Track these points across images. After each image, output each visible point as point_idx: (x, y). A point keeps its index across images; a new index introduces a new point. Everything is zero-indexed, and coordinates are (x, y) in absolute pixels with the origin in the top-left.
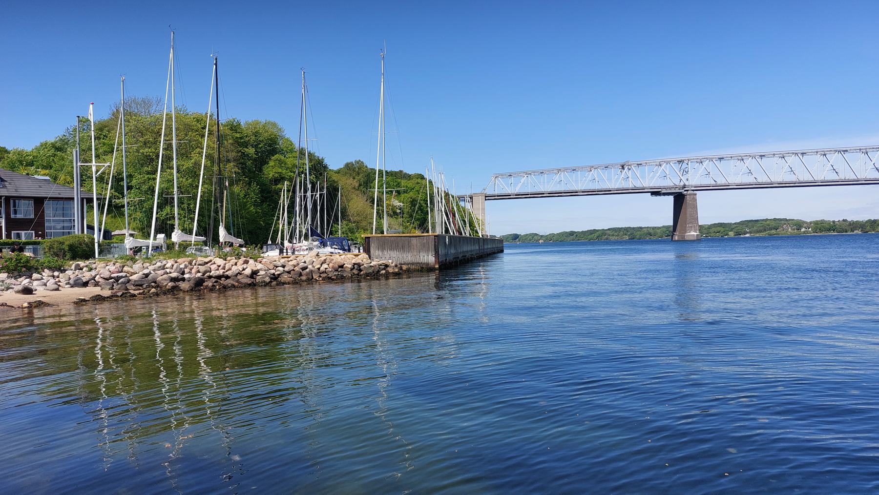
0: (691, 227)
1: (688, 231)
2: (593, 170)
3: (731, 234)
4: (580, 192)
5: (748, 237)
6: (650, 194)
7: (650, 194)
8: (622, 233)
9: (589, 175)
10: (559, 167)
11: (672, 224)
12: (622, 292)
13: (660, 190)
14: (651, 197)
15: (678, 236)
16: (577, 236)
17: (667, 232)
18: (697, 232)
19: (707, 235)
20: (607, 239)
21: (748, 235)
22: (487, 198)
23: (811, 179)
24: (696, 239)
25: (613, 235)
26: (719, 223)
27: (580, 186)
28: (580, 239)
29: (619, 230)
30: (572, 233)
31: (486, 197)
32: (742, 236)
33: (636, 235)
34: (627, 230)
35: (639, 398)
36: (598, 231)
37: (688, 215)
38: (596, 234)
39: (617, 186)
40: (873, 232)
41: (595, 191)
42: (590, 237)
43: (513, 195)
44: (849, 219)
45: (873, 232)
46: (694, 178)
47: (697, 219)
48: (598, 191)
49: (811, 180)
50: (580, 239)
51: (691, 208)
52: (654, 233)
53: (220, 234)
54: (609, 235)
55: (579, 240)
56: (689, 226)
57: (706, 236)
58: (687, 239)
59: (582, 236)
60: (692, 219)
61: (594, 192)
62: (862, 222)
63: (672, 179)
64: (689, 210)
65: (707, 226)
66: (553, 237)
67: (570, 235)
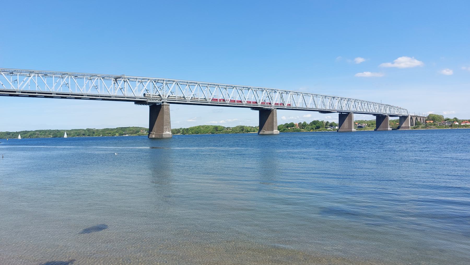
0: (167, 128)
1: (165, 131)
2: (32, 76)
3: (117, 134)
5: (127, 136)
6: (134, 103)
7: (134, 103)
8: (48, 133)
9: (27, 80)
10: (32, 69)
11: (148, 128)
12: (329, 174)
17: (78, 133)
19: (103, 135)
20: (37, 137)
24: (171, 137)
25: (41, 135)
26: (107, 129)
29: (45, 132)
32: (124, 136)
34: (50, 131)
36: (29, 132)
37: (164, 120)
38: (29, 134)
40: (187, 134)
45: (187, 134)
47: (170, 123)
54: (38, 135)
56: (165, 127)
57: (103, 136)
60: (167, 122)
62: (228, 128)
64: (165, 116)
67: (7, 134)
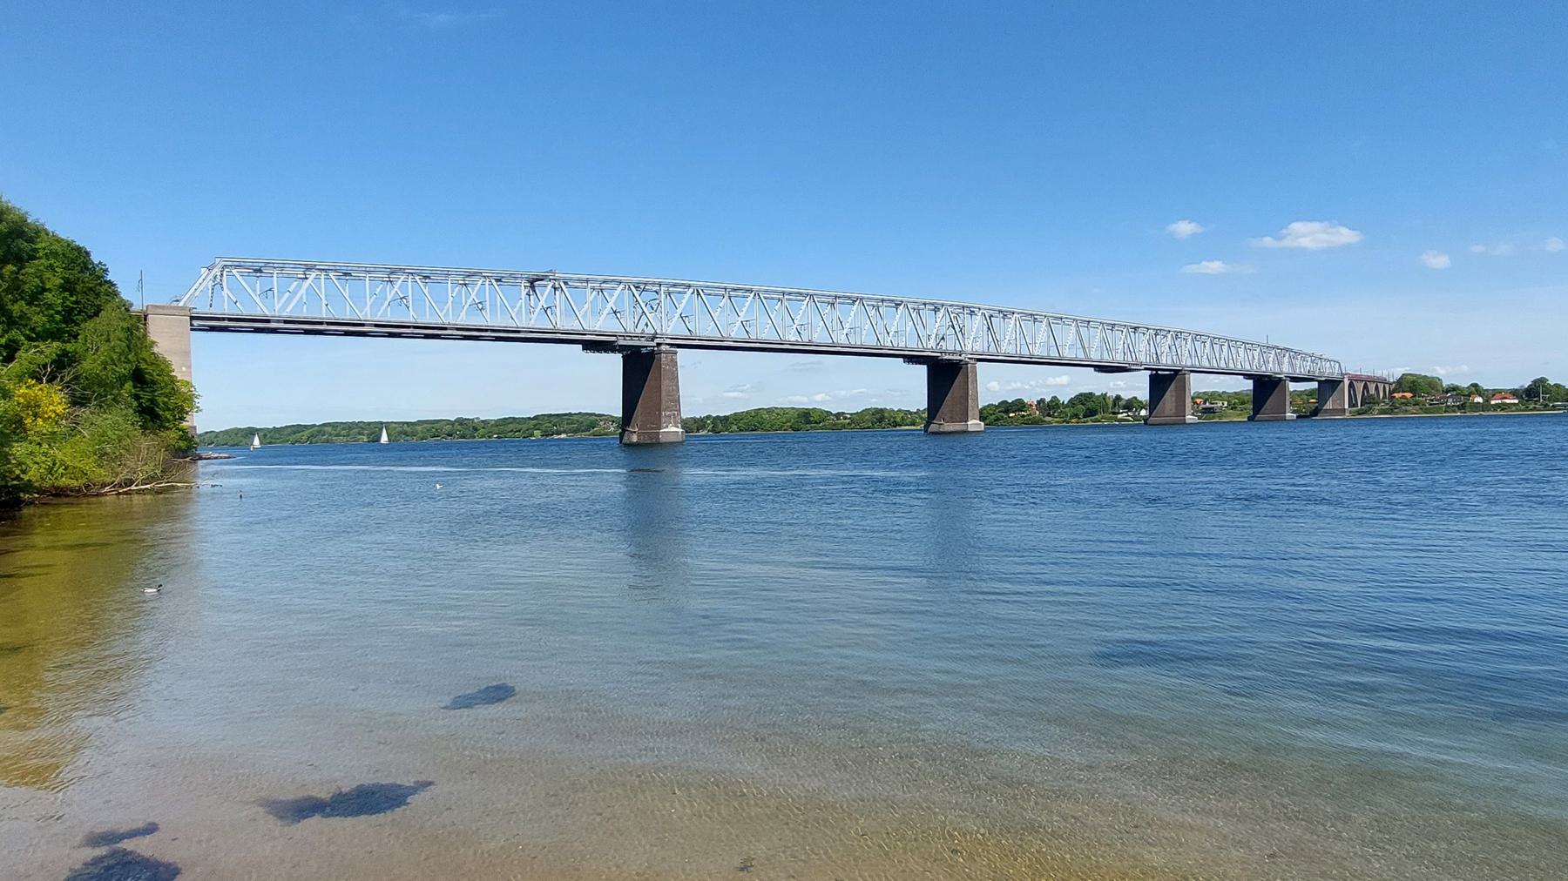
0: (669, 416)
9: (299, 287)
11: (621, 415)
13: (613, 339)
18: (678, 427)
21: (563, 436)
22: (196, 323)
23: (716, 335)
31: (192, 318)
35: (1517, 653)
37: (663, 393)
38: (307, 433)
43: (278, 321)
46: (666, 323)
51: (668, 379)
52: (413, 432)
53: (1268, 402)
58: (664, 440)
63: (935, 336)
64: (665, 383)
65: (493, 422)
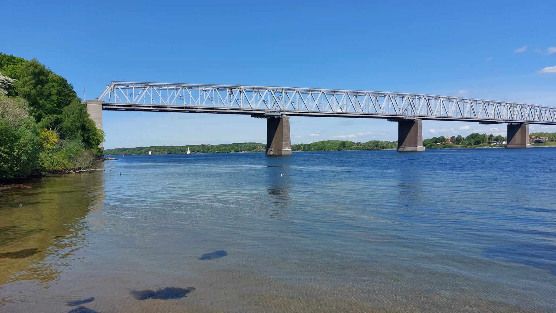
0: (286, 144)
3: (233, 151)
4: (200, 108)
11: (266, 144)
13: (264, 112)
14: (252, 118)
15: (274, 152)
16: (129, 151)
22: (104, 107)
27: (134, 100)
28: (132, 153)
30: (124, 150)
31: (103, 105)
33: (172, 151)
34: (164, 148)
36: (144, 148)
37: (284, 134)
38: (144, 150)
39: (204, 105)
40: (309, 151)
41: (114, 105)
42: (139, 152)
44: (307, 144)
46: (420, 110)
48: (117, 106)
49: (340, 112)
50: (132, 153)
54: (153, 151)
55: (131, 154)
57: (217, 152)
59: (133, 151)
61: (112, 105)
64: (284, 130)
66: (110, 152)
